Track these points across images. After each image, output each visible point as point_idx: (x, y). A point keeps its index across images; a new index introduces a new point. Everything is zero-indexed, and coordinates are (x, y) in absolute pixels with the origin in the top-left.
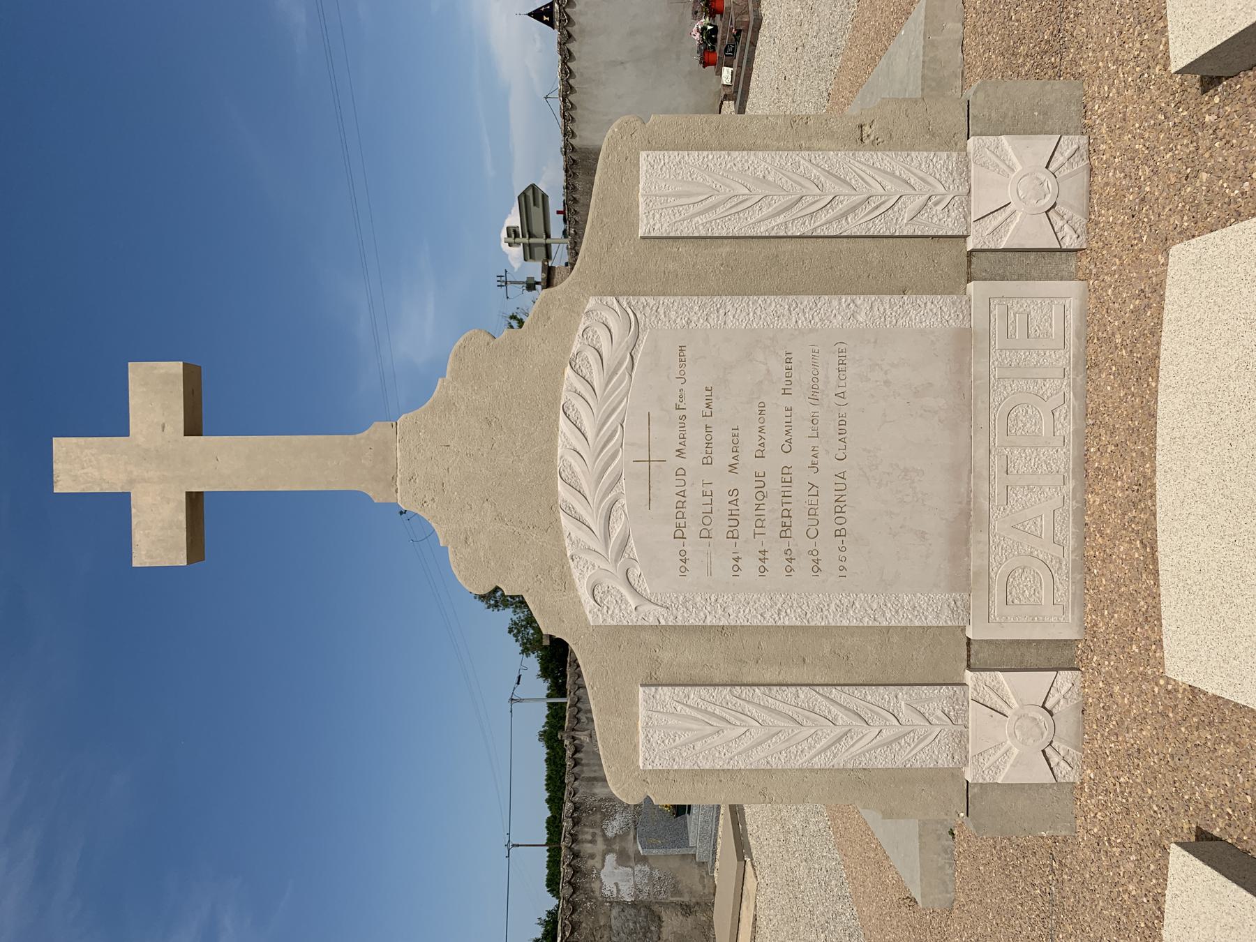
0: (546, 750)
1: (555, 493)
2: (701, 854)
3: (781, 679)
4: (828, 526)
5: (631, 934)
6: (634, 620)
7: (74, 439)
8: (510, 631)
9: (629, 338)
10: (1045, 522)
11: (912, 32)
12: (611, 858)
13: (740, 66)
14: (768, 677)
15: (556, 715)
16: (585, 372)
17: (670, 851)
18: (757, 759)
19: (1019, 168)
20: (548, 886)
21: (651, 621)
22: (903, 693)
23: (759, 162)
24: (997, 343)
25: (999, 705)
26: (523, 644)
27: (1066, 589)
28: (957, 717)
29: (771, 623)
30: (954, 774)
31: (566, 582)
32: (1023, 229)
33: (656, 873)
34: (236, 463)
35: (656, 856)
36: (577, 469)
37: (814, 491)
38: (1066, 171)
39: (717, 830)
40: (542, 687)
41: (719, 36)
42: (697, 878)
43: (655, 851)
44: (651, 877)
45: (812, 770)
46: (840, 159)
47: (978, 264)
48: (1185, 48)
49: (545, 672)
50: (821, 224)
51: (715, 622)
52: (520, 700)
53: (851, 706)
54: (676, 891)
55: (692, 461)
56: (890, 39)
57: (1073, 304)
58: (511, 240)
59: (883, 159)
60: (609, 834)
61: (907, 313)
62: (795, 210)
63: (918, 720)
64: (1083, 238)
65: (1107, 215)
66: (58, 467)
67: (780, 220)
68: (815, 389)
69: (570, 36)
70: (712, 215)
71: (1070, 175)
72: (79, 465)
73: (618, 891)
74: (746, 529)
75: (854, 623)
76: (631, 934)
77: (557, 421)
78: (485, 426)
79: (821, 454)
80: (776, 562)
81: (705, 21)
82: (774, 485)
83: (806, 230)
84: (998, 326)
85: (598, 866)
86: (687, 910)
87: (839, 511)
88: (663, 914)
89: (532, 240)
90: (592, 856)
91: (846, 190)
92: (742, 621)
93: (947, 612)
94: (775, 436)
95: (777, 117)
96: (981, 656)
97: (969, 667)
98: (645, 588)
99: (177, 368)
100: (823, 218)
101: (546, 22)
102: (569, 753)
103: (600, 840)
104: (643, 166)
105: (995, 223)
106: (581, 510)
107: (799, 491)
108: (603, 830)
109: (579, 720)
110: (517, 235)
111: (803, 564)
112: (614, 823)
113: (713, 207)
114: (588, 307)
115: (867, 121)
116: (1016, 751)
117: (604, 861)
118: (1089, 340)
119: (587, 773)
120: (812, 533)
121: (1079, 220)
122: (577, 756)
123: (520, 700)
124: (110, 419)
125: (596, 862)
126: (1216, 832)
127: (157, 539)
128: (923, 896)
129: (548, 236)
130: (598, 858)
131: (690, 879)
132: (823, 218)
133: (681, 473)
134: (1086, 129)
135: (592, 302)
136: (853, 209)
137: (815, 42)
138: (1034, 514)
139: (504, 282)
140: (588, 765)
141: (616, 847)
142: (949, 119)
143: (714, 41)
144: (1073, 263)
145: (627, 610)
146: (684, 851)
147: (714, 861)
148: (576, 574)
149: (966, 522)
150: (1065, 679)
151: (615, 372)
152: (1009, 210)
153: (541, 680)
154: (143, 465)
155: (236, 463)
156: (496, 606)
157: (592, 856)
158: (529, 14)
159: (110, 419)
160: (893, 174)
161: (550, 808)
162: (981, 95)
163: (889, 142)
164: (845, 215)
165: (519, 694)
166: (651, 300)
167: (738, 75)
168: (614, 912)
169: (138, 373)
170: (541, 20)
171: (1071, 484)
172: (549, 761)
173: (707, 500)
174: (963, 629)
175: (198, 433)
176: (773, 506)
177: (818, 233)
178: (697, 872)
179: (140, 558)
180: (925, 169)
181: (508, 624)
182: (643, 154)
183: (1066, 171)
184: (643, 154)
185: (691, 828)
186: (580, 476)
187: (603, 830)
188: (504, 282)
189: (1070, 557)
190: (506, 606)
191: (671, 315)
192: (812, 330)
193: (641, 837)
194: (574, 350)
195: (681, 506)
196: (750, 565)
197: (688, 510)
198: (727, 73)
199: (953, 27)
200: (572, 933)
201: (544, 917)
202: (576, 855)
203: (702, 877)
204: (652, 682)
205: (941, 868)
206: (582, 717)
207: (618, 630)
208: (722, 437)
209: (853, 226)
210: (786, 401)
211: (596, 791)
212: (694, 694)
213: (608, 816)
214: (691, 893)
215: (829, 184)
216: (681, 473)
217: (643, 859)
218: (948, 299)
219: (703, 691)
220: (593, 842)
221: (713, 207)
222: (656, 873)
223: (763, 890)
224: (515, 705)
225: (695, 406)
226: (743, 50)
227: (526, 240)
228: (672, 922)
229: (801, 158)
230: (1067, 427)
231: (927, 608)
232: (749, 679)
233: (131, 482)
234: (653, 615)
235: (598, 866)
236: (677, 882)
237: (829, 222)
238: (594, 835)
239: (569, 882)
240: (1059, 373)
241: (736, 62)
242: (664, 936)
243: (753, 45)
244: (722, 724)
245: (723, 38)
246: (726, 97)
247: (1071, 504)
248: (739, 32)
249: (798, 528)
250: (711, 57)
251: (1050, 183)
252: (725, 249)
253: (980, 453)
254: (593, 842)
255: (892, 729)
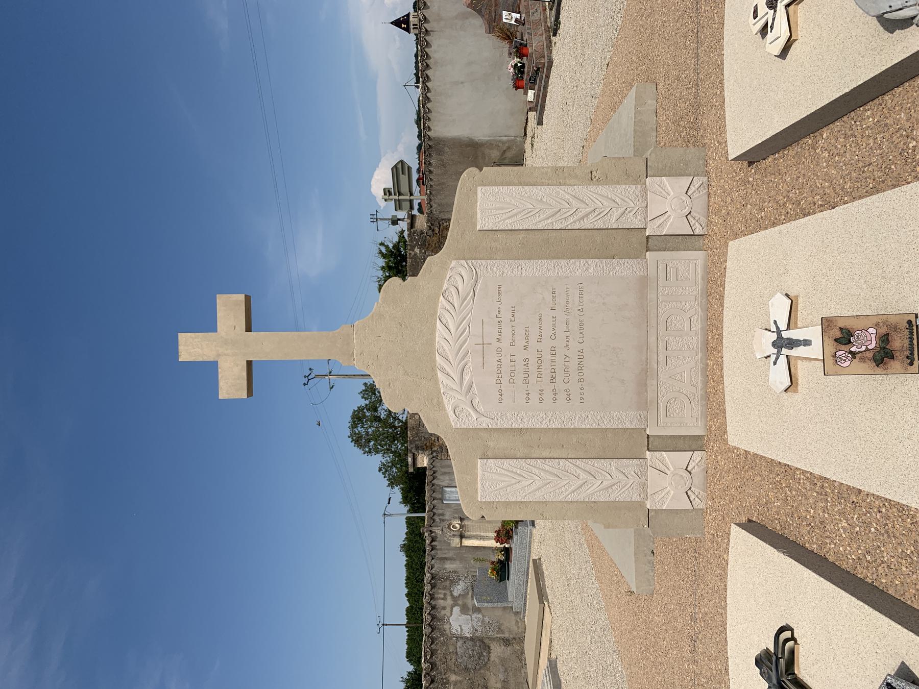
0: (405, 558)
1: (434, 361)
2: (517, 606)
3: (550, 456)
4: (574, 377)
5: (470, 657)
6: (475, 425)
7: (189, 334)
8: (380, 470)
9: (473, 281)
10: (686, 375)
11: (629, 101)
12: (456, 610)
13: (539, 90)
14: (544, 454)
15: (414, 527)
16: (450, 299)
17: (496, 605)
18: (539, 496)
19: (672, 193)
20: (407, 657)
21: (484, 426)
22: (614, 463)
23: (539, 192)
24: (661, 283)
25: (664, 469)
26: (389, 480)
27: (697, 410)
28: (642, 475)
29: (545, 426)
30: (641, 505)
31: (441, 406)
32: (674, 225)
33: (487, 619)
34: (267, 346)
35: (486, 608)
36: (446, 348)
37: (567, 359)
38: (696, 195)
39: (526, 590)
40: (402, 511)
41: (526, 70)
42: (514, 622)
43: (486, 605)
44: (483, 621)
45: (567, 502)
46: (583, 191)
47: (650, 243)
48: (736, 148)
49: (406, 500)
50: (571, 223)
51: (517, 426)
52: (390, 515)
53: (587, 469)
54: (500, 631)
55: (505, 344)
56: (624, 97)
57: (700, 263)
58: (387, 197)
59: (602, 190)
60: (455, 594)
61: (614, 268)
62: (557, 216)
63: (622, 477)
64: (705, 229)
65: (715, 219)
66: (181, 348)
67: (549, 221)
68: (567, 307)
69: (428, 66)
70: (514, 219)
71: (698, 197)
72: (192, 347)
73: (462, 630)
74: (533, 379)
75: (588, 426)
76: (470, 657)
77: (435, 324)
78: (399, 326)
79: (571, 338)
80: (548, 395)
81: (517, 60)
82: (547, 356)
83: (563, 226)
84: (661, 274)
85: (448, 614)
86: (507, 642)
87: (580, 369)
88: (492, 647)
89: (401, 197)
90: (444, 608)
91: (583, 206)
92: (530, 426)
93: (636, 421)
94: (547, 332)
95: (548, 167)
96: (652, 443)
97: (648, 450)
98: (481, 408)
99: (241, 297)
100: (571, 220)
101: (404, 29)
102: (428, 542)
103: (449, 598)
104: (479, 194)
105: (660, 222)
106: (448, 369)
107: (559, 359)
108: (451, 592)
109: (434, 520)
110: (390, 194)
111: (562, 396)
112: (459, 587)
113: (516, 215)
114: (452, 266)
115: (594, 169)
116: (672, 492)
117: (452, 611)
118: (708, 281)
119: (440, 554)
120: (566, 381)
121: (703, 220)
122: (434, 543)
123: (390, 515)
124: (208, 324)
125: (446, 612)
126: (754, 519)
127: (231, 384)
128: (637, 588)
129: (411, 194)
130: (448, 609)
131: (509, 622)
132: (571, 220)
133: (499, 350)
134: (707, 174)
135: (454, 263)
136: (587, 215)
137: (583, 86)
138: (679, 370)
139: (375, 219)
140: (441, 549)
141: (460, 602)
142: (641, 168)
143: (523, 73)
144: (701, 241)
145: (472, 420)
146: (505, 604)
147: (525, 612)
148: (445, 402)
149: (645, 376)
150: (698, 455)
151: (465, 299)
152: (667, 215)
153: (403, 505)
154: (220, 347)
155: (267, 346)
156: (370, 452)
157: (444, 608)
158: (392, 23)
159: (208, 324)
160: (607, 197)
161: (409, 600)
162: (653, 155)
163: (606, 180)
164: (583, 218)
165: (389, 511)
166: (483, 262)
167: (538, 96)
168: (459, 644)
169: (221, 299)
170: (400, 27)
171: (700, 355)
172: (408, 566)
173: (513, 364)
174: (645, 430)
175: (251, 331)
176: (546, 366)
177: (569, 227)
178: (513, 618)
179: (222, 395)
180: (627, 193)
181: (378, 465)
182: (479, 188)
183: (696, 195)
184: (479, 188)
185: (510, 590)
186: (448, 352)
187: (451, 592)
188: (375, 219)
189: (700, 392)
190: (377, 452)
191: (495, 270)
192: (566, 277)
193: (476, 595)
194: (444, 288)
195: (499, 367)
196: (535, 397)
197: (503, 369)
198: (531, 94)
199: (651, 102)
200: (431, 657)
201: (406, 676)
202: (433, 608)
203: (517, 622)
204: (485, 457)
205: (647, 572)
206: (437, 518)
207: (467, 430)
208: (520, 331)
209: (586, 224)
210: (553, 313)
211: (447, 566)
212: (506, 463)
213: (454, 582)
214: (510, 631)
215: (574, 202)
216: (499, 350)
217: (477, 610)
218: (636, 261)
219: (510, 461)
220: (444, 599)
221: (516, 215)
222: (487, 619)
223: (557, 622)
224: (387, 518)
225: (506, 316)
226: (541, 80)
227: (396, 197)
228: (497, 651)
229: (560, 190)
230: (697, 326)
231: (627, 419)
232: (534, 456)
233: (219, 355)
234: (485, 423)
235: (448, 614)
236: (501, 625)
237: (575, 222)
238: (445, 594)
239: (429, 614)
240: (693, 298)
241: (536, 87)
242: (492, 659)
243: (548, 77)
244: (521, 478)
245: (528, 72)
246: (530, 109)
247: (700, 366)
248: (538, 69)
249: (559, 379)
250: (521, 83)
251: (688, 200)
252: (521, 236)
253: (652, 339)
254: (444, 599)
255: (608, 480)
